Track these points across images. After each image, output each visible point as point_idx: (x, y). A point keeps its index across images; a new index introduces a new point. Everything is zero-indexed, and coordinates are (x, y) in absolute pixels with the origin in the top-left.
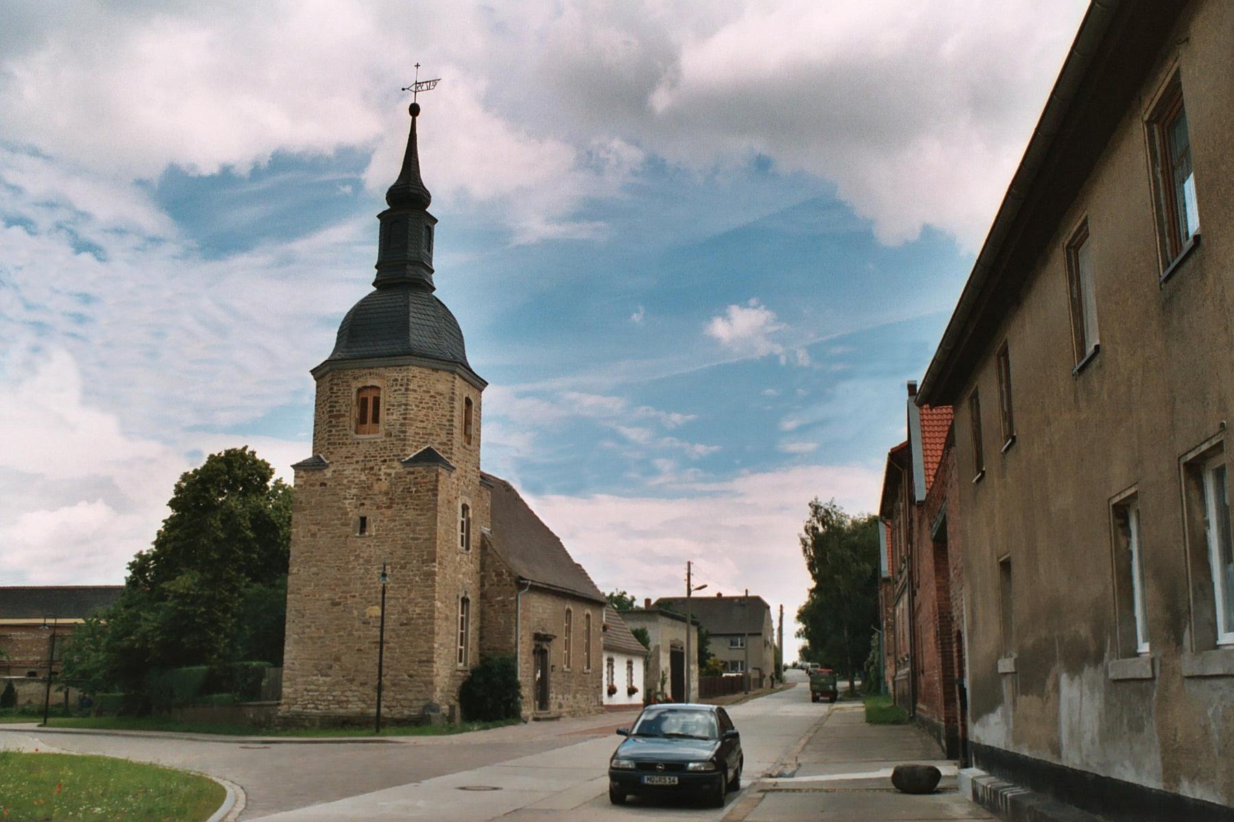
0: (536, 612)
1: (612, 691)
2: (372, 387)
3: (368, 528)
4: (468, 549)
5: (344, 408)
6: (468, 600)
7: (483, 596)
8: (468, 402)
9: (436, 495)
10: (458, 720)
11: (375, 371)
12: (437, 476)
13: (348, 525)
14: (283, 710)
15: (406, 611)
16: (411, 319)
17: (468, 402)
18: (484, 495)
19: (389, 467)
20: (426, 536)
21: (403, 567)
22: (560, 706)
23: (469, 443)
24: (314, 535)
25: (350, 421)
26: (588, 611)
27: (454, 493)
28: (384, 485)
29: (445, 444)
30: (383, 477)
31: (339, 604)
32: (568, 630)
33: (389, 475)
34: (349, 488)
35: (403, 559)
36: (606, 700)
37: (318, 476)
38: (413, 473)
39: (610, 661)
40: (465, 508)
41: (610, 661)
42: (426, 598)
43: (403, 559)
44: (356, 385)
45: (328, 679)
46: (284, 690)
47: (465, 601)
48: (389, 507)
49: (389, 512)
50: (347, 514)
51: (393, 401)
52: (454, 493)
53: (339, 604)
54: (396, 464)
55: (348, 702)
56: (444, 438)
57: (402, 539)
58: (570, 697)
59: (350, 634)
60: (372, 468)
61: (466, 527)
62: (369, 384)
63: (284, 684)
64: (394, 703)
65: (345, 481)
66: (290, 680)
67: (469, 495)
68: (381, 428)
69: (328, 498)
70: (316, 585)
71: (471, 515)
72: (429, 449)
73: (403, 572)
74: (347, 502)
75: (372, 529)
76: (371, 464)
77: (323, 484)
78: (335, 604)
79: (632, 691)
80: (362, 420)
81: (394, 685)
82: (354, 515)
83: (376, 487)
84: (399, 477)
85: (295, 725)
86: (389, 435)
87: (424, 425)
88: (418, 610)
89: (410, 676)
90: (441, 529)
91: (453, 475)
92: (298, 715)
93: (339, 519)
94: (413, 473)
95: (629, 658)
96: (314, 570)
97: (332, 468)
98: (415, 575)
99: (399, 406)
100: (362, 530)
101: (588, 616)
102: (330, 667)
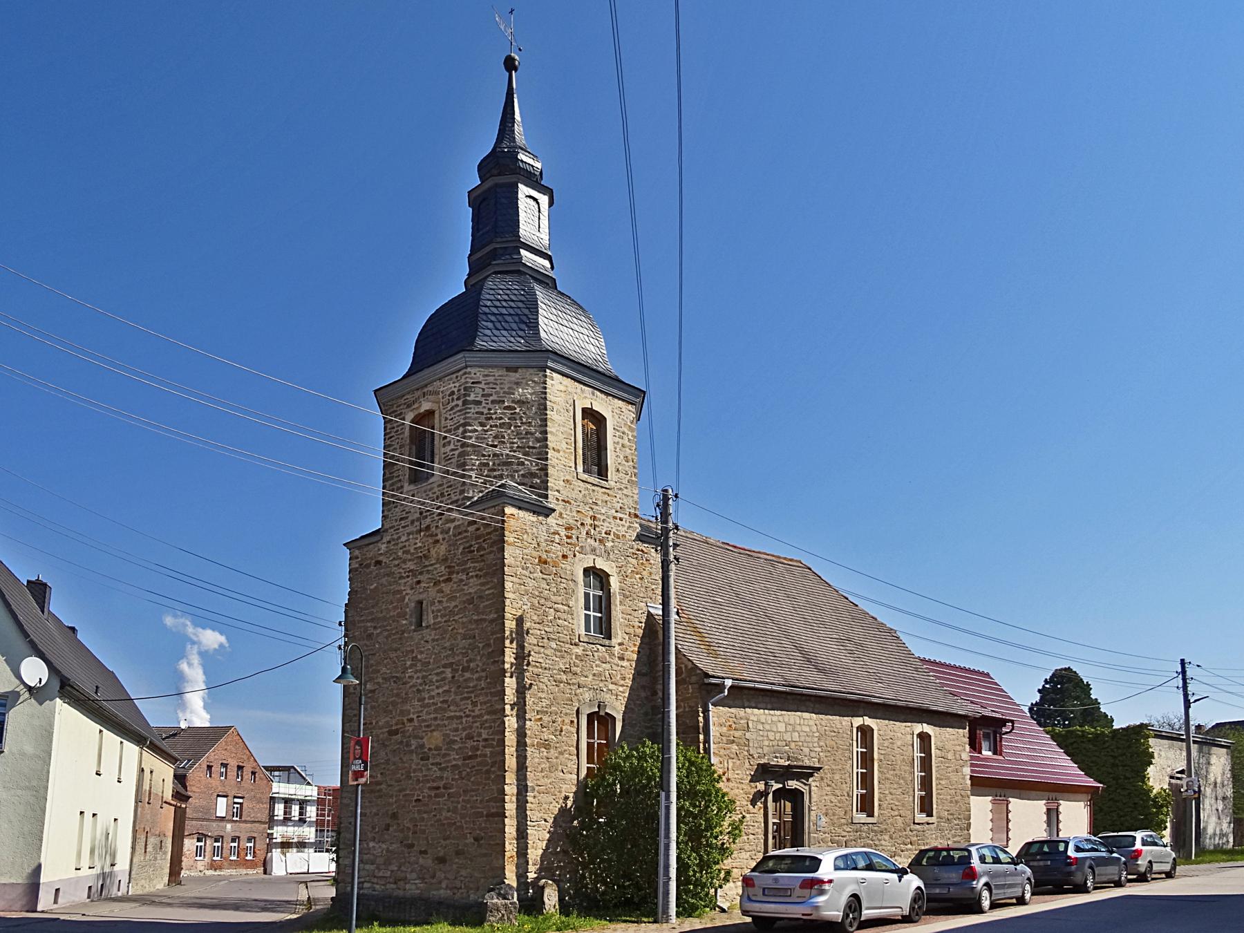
9: (503, 550)
11: (430, 388)
28: (442, 549)
30: (440, 537)
34: (404, 562)
35: (466, 654)
44: (410, 416)
45: (384, 846)
56: (531, 464)
60: (428, 528)
82: (410, 598)
95: (1053, 795)
102: (387, 827)
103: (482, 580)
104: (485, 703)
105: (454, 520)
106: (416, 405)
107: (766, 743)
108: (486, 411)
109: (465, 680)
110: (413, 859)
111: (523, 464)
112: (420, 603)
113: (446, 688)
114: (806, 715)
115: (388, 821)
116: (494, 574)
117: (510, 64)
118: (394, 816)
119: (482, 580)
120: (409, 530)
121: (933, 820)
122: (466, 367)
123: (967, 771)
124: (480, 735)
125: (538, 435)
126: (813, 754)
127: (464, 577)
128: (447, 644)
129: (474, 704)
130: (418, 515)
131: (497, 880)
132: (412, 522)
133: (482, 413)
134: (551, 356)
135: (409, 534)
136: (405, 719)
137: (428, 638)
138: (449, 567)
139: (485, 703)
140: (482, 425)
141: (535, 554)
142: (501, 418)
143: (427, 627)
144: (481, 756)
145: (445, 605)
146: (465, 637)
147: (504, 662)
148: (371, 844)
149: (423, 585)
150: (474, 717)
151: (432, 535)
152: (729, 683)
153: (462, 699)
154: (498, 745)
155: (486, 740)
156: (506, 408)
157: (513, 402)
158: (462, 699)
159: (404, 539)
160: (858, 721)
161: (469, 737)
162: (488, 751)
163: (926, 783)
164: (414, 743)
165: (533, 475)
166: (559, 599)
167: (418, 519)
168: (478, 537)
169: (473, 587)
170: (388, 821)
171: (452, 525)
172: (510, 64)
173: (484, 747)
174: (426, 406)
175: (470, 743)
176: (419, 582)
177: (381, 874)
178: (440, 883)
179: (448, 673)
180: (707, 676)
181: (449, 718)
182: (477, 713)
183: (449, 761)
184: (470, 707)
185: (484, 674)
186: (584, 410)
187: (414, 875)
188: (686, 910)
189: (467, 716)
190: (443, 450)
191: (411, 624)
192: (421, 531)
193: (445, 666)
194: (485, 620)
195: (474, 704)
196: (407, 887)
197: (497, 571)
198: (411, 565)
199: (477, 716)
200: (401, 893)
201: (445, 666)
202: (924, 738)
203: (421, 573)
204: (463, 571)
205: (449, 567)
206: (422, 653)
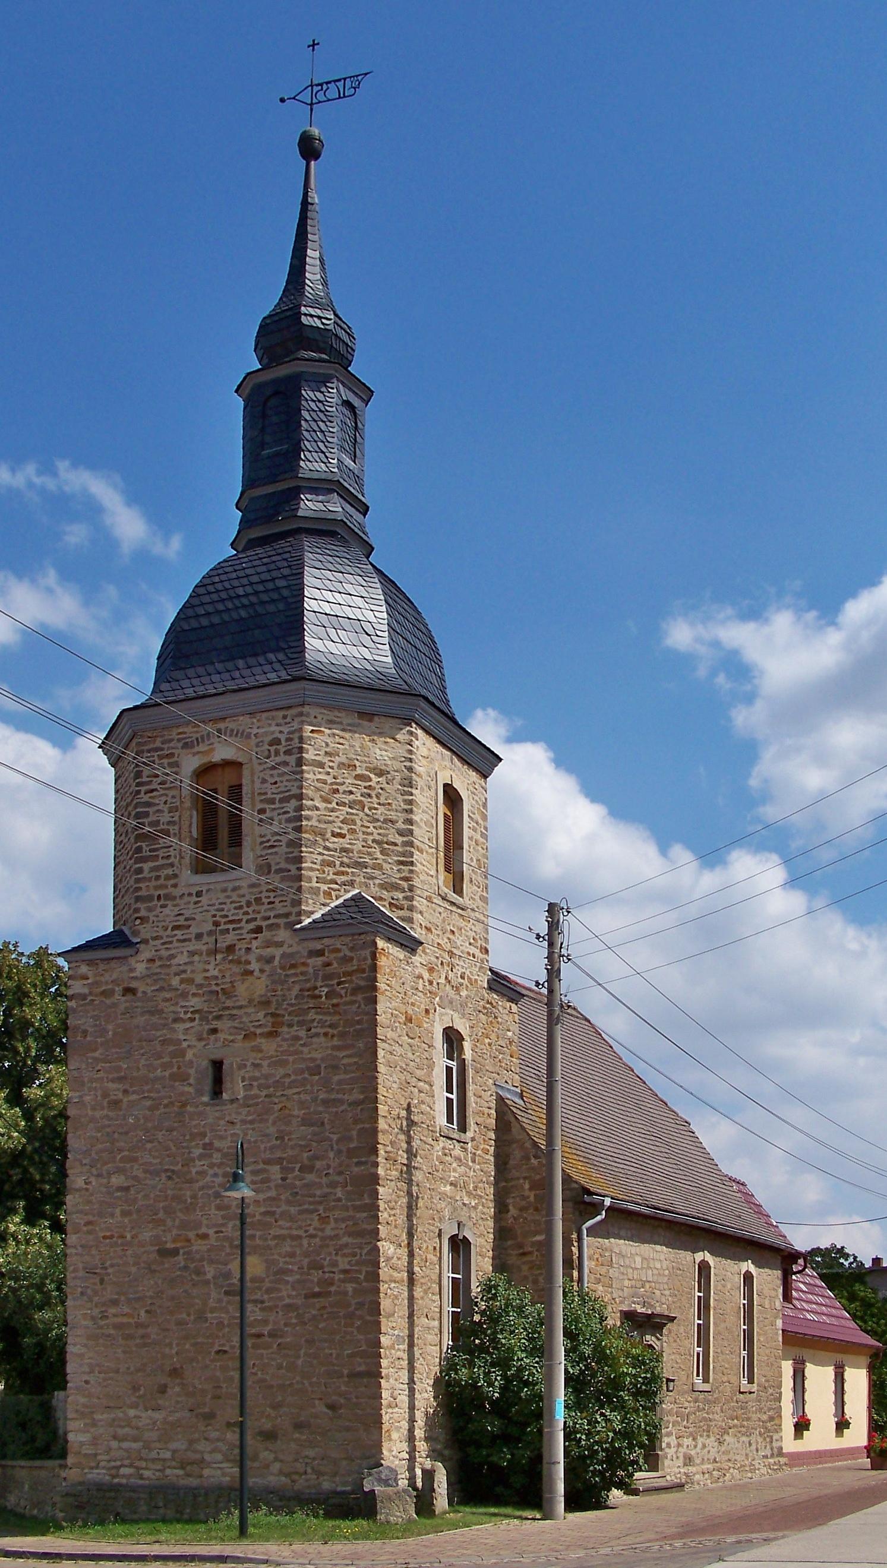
0: (627, 1272)
1: (802, 1426)
2: (227, 764)
3: (227, 1084)
4: (463, 1128)
5: (165, 817)
6: (466, 1242)
7: (502, 1234)
8: (452, 798)
9: (374, 1001)
10: (441, 1501)
11: (231, 725)
12: (374, 957)
13: (183, 1078)
14: (74, 1472)
15: (316, 1266)
16: (309, 604)
17: (452, 798)
18: (503, 1016)
19: (268, 944)
20: (357, 1096)
21: (306, 1169)
22: (689, 1460)
23: (458, 890)
24: (115, 1104)
25: (182, 846)
26: (748, 1266)
27: (421, 1001)
28: (259, 986)
29: (395, 887)
30: (255, 966)
31: (175, 1252)
32: (704, 1307)
33: (270, 960)
34: (184, 995)
35: (307, 1148)
36: (790, 1444)
37: (118, 971)
38: (320, 953)
39: (799, 1376)
40: (453, 1038)
41: (799, 1376)
42: (360, 1234)
43: (307, 1148)
44: (190, 763)
45: (157, 1415)
46: (71, 1437)
47: (460, 1246)
48: (272, 1034)
49: (270, 1047)
50: (182, 1053)
51: (270, 789)
52: (421, 1001)
53: (175, 1252)
54: (283, 935)
55: (201, 1463)
56: (392, 871)
57: (302, 1104)
58: (711, 1441)
59: (201, 1317)
60: (230, 949)
61: (458, 1081)
62: (217, 757)
63: (71, 1425)
64: (300, 1467)
65: (175, 981)
66: (82, 1415)
67: (461, 1008)
68: (248, 856)
69: (141, 1020)
70: (124, 1214)
71: (468, 1054)
72: (358, 899)
73: (310, 1177)
74: (181, 1027)
75: (236, 1087)
76: (230, 938)
77: (129, 991)
78: (165, 1253)
79: (842, 1425)
80: (208, 841)
81: (298, 1426)
82: (197, 1055)
83: (242, 989)
84: (291, 963)
85: (102, 1506)
86: (265, 869)
87: (343, 843)
88: (343, 1263)
89: (332, 1407)
90: (388, 1082)
91: (417, 959)
92: (100, 1487)
93: (165, 1066)
94: (320, 953)
95: (839, 1357)
96: (117, 1180)
97: (146, 953)
98: (333, 1185)
99: (286, 800)
100: (217, 1090)
101: (748, 1278)
102: (163, 1390)
103: (336, 1042)
104: (343, 1220)
105: (279, 944)
106: (202, 748)
107: (626, 1283)
108: (330, 780)
109: (306, 1185)
110: (215, 1435)
111: (379, 867)
112: (218, 1066)
113: (273, 1193)
114: (658, 1247)
115: (163, 1379)
116: (359, 1034)
117: (309, 148)
118: (175, 1373)
119: (336, 1042)
120: (193, 946)
121: (754, 1387)
122: (303, 705)
123: (779, 1323)
124: (335, 1264)
125: (400, 825)
126: (663, 1300)
127: (302, 1033)
128: (272, 1130)
129: (324, 1220)
130: (210, 927)
131: (372, 1461)
132: (199, 936)
133: (325, 782)
134: (423, 704)
135: (192, 954)
136: (191, 1235)
137: (233, 1117)
138: (273, 1015)
139: (343, 1220)
140: (326, 800)
141: (403, 1008)
142: (351, 792)
143: (232, 1101)
144: (337, 1293)
145: (265, 1070)
146: (306, 1122)
147: (377, 1165)
148: (132, 1412)
149: (221, 1036)
150: (323, 1239)
151: (239, 962)
152: (608, 1202)
153: (301, 1212)
154: (366, 1280)
155: (345, 1272)
156: (358, 777)
157: (368, 769)
158: (301, 1212)
159: (182, 959)
160: (699, 1256)
161: (316, 1266)
162: (350, 1287)
163: (749, 1337)
164: (210, 1272)
165: (395, 887)
166: (419, 1073)
167: (210, 933)
168: (327, 977)
169: (319, 1049)
170: (163, 1379)
171: (278, 952)
172: (309, 148)
173: (343, 1281)
174: (222, 753)
175: (316, 1275)
176: (214, 1031)
177: (153, 1455)
178: (267, 1466)
179: (275, 1171)
180: (590, 1193)
181: (275, 1237)
182: (328, 1232)
183: (281, 1298)
184: (316, 1223)
185: (340, 1179)
186: (446, 785)
187: (219, 1457)
188: (577, 1501)
189: (312, 1236)
190: (258, 830)
191: (200, 1093)
192: (216, 951)
193: (267, 1162)
194: (341, 1102)
195: (324, 1220)
196: (206, 1472)
197: (365, 1032)
198: (195, 1002)
199: (331, 1238)
200: (193, 1482)
201: (267, 1162)
202: (748, 1278)
203: (219, 1018)
204: (301, 1023)
205: (273, 1015)
206: (221, 1138)
